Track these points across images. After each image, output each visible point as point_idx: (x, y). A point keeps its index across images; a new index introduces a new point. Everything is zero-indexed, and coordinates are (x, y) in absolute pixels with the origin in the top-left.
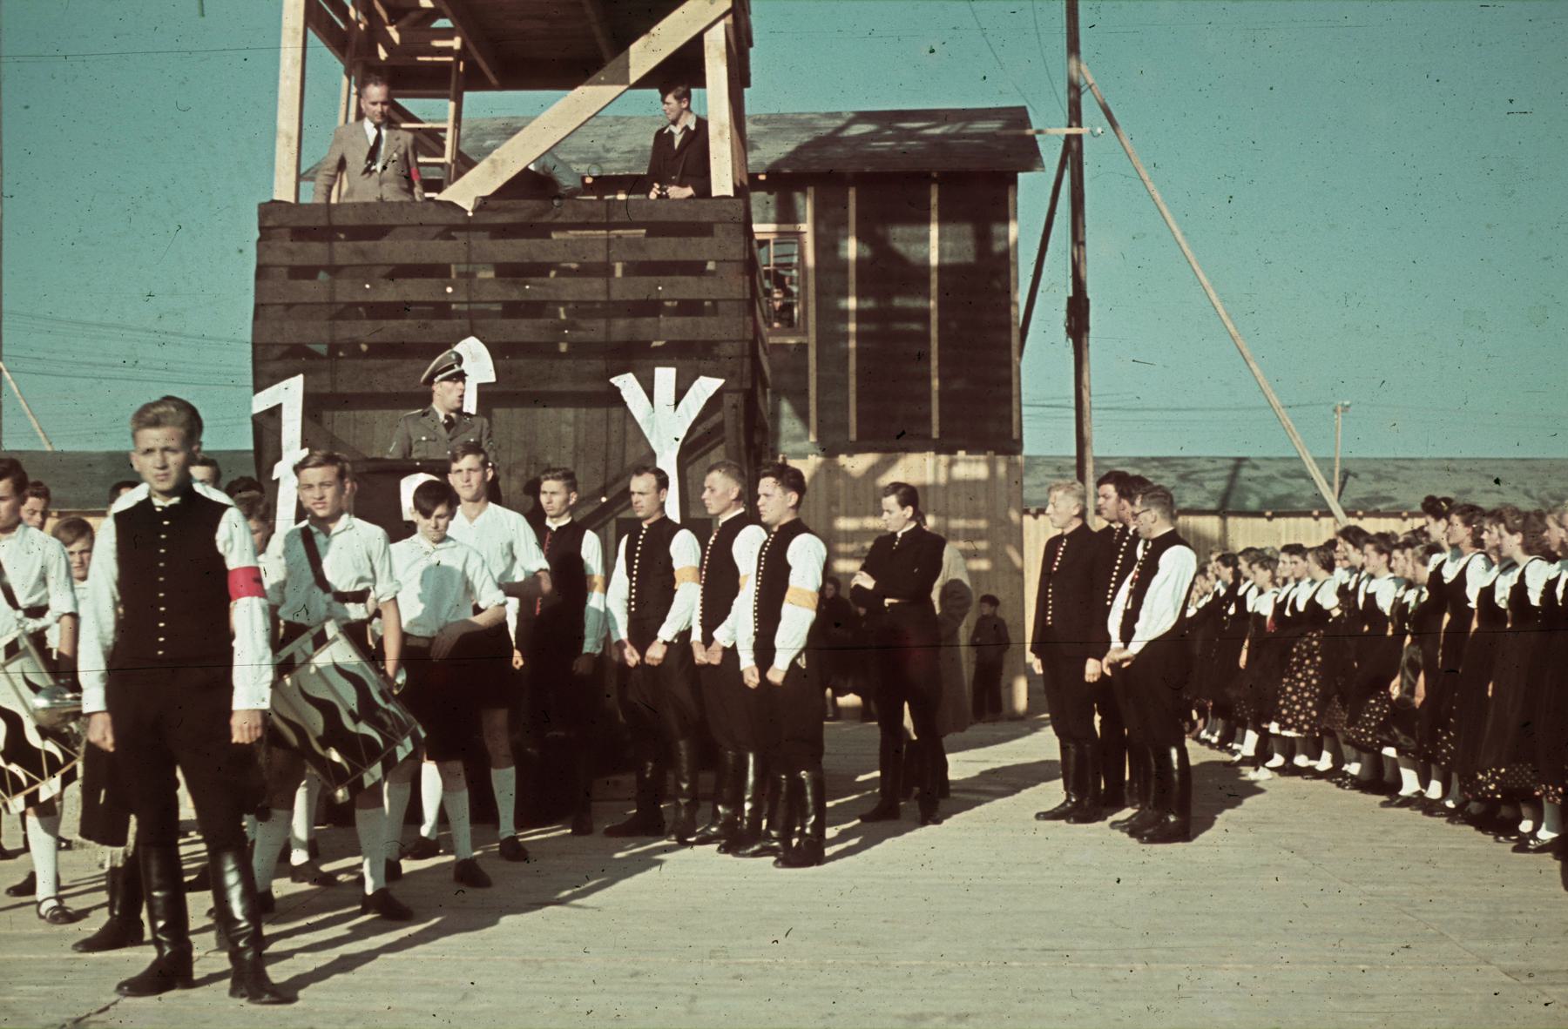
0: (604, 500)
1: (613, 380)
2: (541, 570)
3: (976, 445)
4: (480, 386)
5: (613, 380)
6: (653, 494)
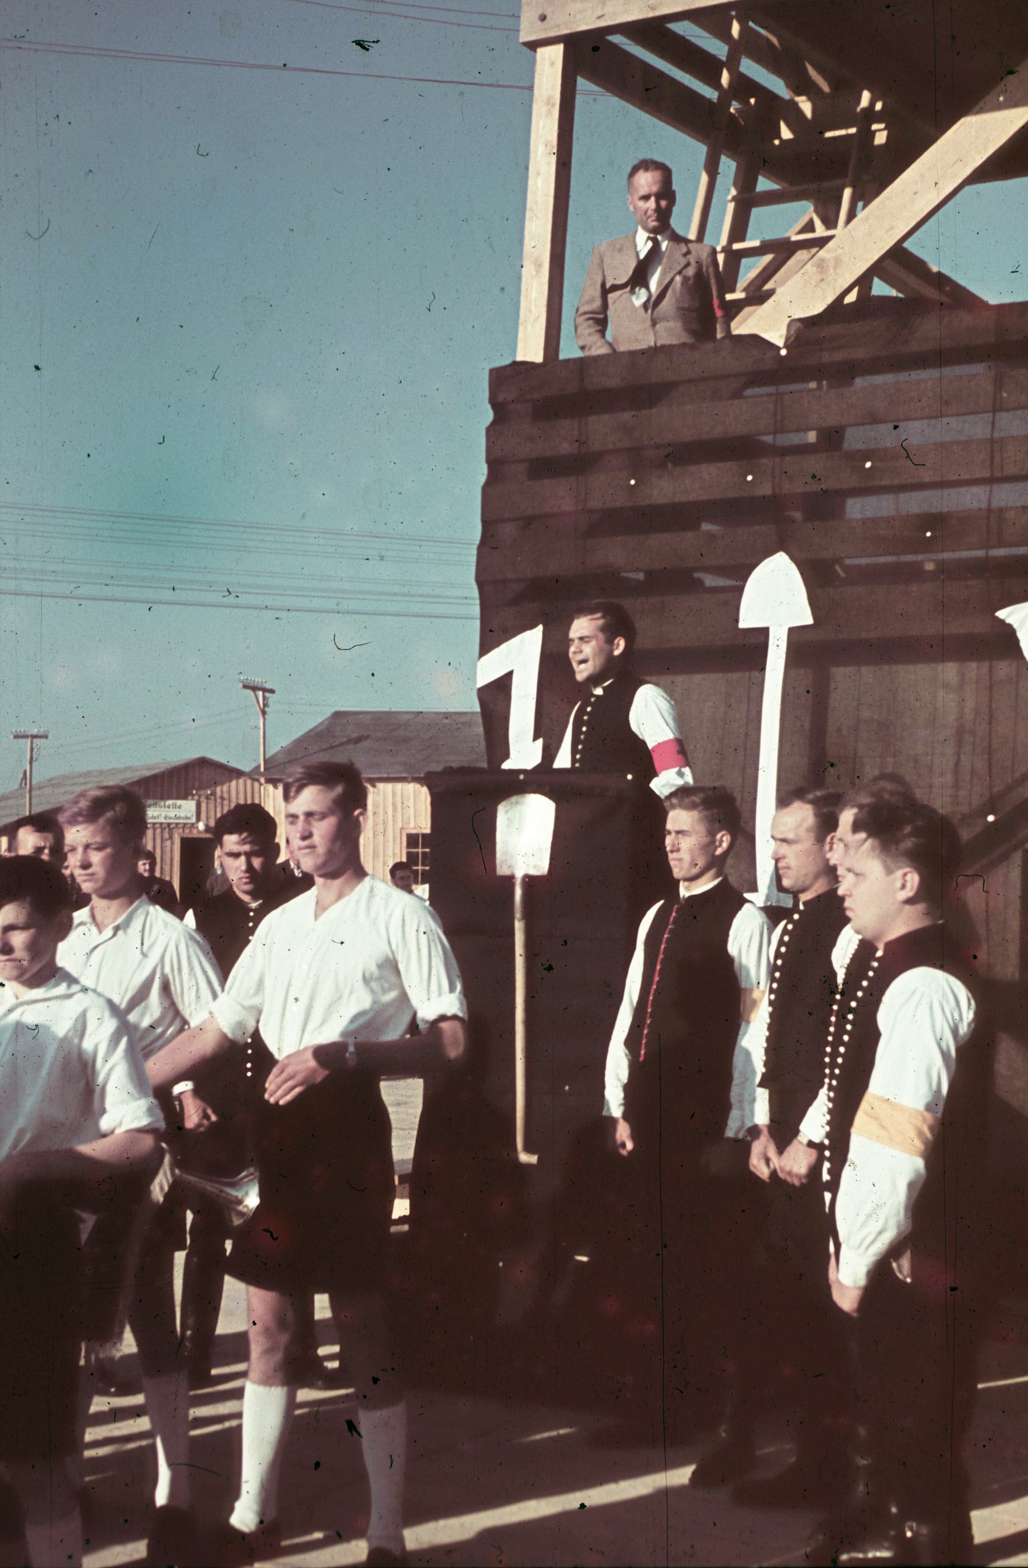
0: (991, 818)
1: (1001, 614)
2: (443, 1018)
3: (289, 865)
4: (792, 631)
5: (1001, 614)
6: (808, 842)
